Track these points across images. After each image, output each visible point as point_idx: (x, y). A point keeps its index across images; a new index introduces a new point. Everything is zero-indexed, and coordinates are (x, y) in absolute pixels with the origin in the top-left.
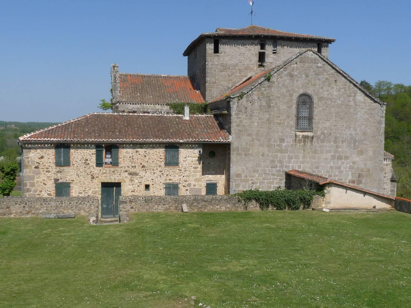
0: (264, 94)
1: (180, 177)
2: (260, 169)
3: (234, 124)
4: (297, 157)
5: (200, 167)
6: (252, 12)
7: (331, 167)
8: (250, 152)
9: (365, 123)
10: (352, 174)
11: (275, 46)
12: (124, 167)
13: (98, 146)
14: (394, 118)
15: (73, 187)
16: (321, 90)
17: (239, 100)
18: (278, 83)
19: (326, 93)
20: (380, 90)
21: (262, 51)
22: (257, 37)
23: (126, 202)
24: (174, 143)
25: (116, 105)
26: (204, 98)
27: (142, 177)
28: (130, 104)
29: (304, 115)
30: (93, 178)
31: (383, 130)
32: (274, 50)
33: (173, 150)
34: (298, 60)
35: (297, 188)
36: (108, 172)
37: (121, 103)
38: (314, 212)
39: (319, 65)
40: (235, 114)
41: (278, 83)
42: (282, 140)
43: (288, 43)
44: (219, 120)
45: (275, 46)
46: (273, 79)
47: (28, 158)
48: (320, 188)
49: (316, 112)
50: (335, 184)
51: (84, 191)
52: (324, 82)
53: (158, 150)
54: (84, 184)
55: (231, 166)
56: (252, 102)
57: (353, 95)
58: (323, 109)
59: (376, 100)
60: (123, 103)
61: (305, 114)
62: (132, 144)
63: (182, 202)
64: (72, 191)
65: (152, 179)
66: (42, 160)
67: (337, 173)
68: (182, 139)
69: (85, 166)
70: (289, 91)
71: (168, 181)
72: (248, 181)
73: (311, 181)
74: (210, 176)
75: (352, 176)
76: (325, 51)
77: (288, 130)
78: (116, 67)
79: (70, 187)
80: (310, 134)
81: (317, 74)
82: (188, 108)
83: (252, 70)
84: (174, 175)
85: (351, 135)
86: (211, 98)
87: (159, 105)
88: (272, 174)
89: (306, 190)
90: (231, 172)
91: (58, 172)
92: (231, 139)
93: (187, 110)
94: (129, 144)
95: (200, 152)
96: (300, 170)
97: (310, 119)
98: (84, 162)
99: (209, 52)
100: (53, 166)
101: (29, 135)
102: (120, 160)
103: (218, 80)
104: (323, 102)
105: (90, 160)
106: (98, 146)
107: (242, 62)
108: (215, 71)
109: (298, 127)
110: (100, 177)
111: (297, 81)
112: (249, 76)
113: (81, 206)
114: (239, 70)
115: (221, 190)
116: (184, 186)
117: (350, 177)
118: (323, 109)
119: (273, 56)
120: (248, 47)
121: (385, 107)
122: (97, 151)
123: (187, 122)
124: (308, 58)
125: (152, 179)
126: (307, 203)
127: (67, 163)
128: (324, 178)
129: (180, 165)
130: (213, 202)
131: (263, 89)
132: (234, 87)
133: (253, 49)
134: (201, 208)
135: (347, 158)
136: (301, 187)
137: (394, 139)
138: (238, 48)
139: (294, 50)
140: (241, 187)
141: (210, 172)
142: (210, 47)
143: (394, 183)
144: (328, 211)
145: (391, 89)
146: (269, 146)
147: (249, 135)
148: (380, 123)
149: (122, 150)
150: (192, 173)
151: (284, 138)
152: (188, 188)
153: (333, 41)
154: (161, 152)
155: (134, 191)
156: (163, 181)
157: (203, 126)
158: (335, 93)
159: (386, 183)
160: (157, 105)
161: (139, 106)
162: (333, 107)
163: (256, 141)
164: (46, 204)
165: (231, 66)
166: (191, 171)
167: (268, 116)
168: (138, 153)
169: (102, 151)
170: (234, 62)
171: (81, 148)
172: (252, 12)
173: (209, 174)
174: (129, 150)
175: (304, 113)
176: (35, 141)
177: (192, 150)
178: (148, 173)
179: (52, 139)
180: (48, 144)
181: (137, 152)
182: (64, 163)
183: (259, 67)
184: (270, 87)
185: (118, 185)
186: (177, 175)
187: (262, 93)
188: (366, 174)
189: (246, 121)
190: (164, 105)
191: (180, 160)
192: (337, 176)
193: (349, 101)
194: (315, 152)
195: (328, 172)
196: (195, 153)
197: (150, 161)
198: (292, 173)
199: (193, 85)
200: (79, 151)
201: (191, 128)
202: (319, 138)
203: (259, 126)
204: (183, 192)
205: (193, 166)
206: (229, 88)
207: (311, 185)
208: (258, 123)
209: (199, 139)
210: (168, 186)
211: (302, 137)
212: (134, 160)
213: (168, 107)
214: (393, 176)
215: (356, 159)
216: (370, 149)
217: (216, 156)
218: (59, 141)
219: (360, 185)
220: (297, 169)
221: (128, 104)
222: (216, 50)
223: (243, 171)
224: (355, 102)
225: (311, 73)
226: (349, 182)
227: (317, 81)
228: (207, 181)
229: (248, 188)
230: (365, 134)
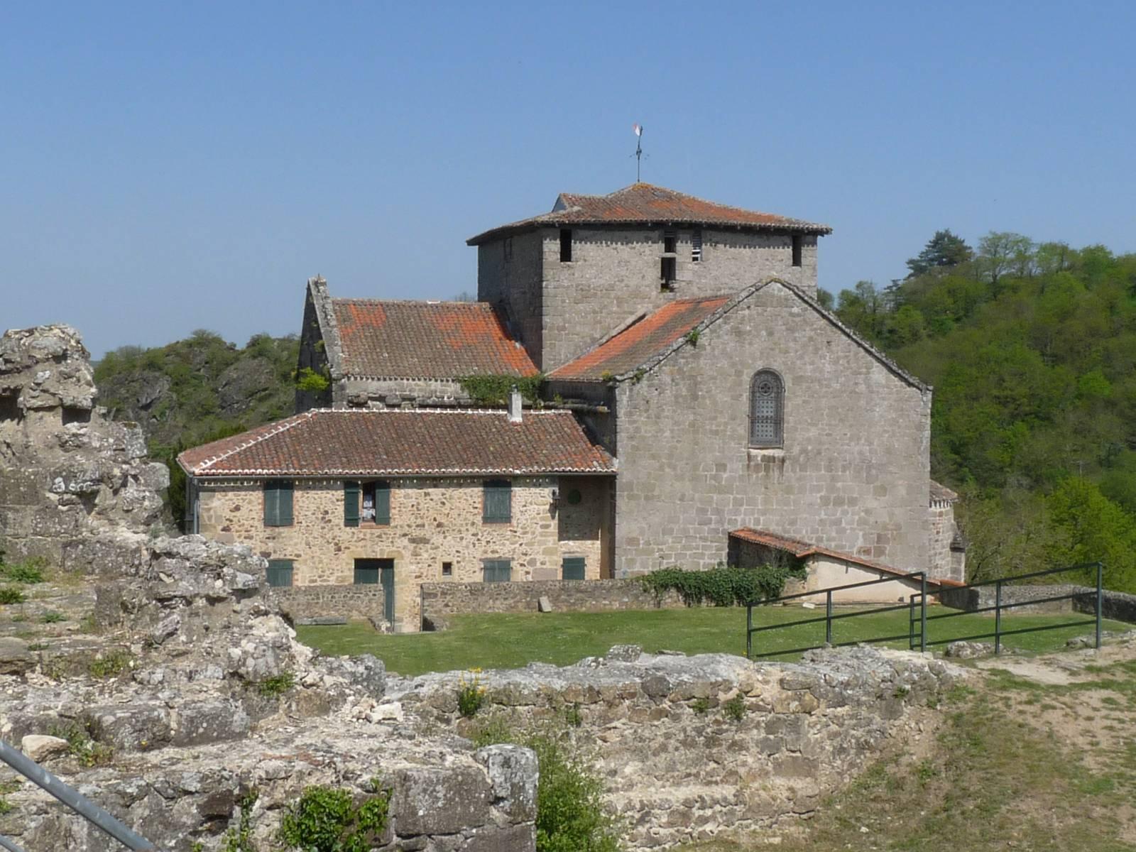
0: (684, 372)
1: (513, 547)
2: (676, 527)
3: (623, 434)
4: (751, 502)
5: (554, 524)
6: (639, 152)
7: (821, 520)
8: (656, 493)
9: (890, 429)
10: (864, 535)
11: (698, 244)
12: (401, 527)
13: (349, 484)
14: (1038, 353)
15: (298, 569)
16: (798, 362)
17: (633, 384)
18: (713, 349)
19: (809, 367)
20: (995, 263)
21: (669, 255)
22: (658, 225)
23: (435, 595)
24: (502, 476)
25: (339, 383)
26: (538, 364)
27: (437, 548)
28: (373, 379)
29: (765, 414)
30: (339, 550)
31: (926, 443)
32: (694, 253)
33: (500, 489)
34: (751, 300)
35: (753, 566)
36: (368, 536)
37: (352, 379)
38: (787, 609)
39: (795, 310)
40: (625, 414)
41: (713, 349)
42: (721, 467)
43: (728, 235)
44: (584, 423)
45: (698, 244)
46: (703, 341)
47: (209, 509)
48: (797, 564)
49: (789, 406)
50: (826, 555)
51: (320, 577)
52: (804, 346)
53: (468, 490)
54: (321, 562)
55: (617, 521)
56: (660, 389)
57: (864, 370)
58: (804, 402)
59: (911, 380)
60: (356, 379)
61: (767, 410)
62: (416, 478)
63: (540, 594)
64: (296, 577)
65: (458, 552)
66: (238, 514)
67: (834, 534)
68: (519, 468)
69: (323, 525)
70: (733, 365)
71: (490, 555)
72: (652, 552)
73: (781, 551)
74: (571, 543)
75: (865, 539)
76: (810, 253)
77: (733, 445)
78: (324, 284)
79: (292, 569)
80: (777, 453)
81: (791, 330)
82: (520, 397)
83: (644, 297)
84: (501, 543)
85: (861, 453)
86: (554, 365)
87: (436, 381)
88: (701, 538)
89: (772, 567)
90: (617, 534)
91: (268, 538)
92: (616, 465)
93: (517, 400)
94: (411, 479)
95: (554, 493)
96: (759, 528)
97: (778, 421)
98: (320, 516)
99: (550, 259)
100: (260, 525)
101: (209, 463)
102: (393, 511)
103: (569, 322)
104: (804, 385)
105: (333, 513)
106: (349, 484)
107: (623, 280)
108: (563, 301)
109: (755, 439)
110: (353, 548)
111: (750, 344)
112: (640, 314)
113: (352, 602)
114: (617, 298)
115: (593, 570)
116: (522, 565)
117: (860, 543)
118: (804, 402)
119: (692, 266)
120: (638, 246)
121: (930, 395)
122: (346, 493)
123: (518, 428)
124: (773, 296)
125: (458, 552)
126: (773, 593)
127: (287, 520)
128: (805, 545)
129: (514, 522)
130: (597, 593)
131: (682, 361)
132: (606, 338)
133: (647, 252)
134: (574, 604)
135: (853, 502)
136: (761, 562)
137: (1037, 422)
138: (616, 249)
139: (739, 253)
140: (638, 564)
141: (570, 535)
142: (552, 248)
143: (957, 554)
144: (812, 606)
145: (1030, 258)
146: (695, 479)
147: (653, 457)
148: (920, 427)
149: (397, 491)
150: (539, 538)
151: (724, 461)
152: (530, 569)
153: (827, 232)
154: (475, 495)
155: (420, 577)
156: (479, 556)
157: (554, 436)
158: (828, 368)
159: (940, 553)
160: (433, 382)
161: (392, 384)
162: (824, 397)
163: (667, 470)
164: (288, 599)
165: (598, 293)
166: (537, 533)
167: (692, 417)
168: (428, 498)
169: (357, 493)
170: (605, 280)
171: (314, 489)
172: (639, 152)
173: (569, 539)
174: (410, 491)
175: (765, 410)
176: (226, 474)
177: (538, 490)
178: (449, 538)
179: (259, 471)
180: (249, 480)
181: (427, 494)
182: (281, 520)
183: (662, 291)
184: (696, 357)
185: (388, 564)
186: (507, 542)
187: (680, 371)
188: (892, 534)
189: (648, 428)
190: (448, 381)
191: (513, 510)
192: (834, 539)
193: (856, 384)
194: (789, 490)
195: (814, 531)
196: (545, 495)
197: (454, 513)
198: (742, 535)
199: (503, 327)
200: (312, 493)
201: (531, 442)
202: (795, 460)
203: (673, 437)
204: (519, 575)
205: (541, 523)
206: (594, 340)
207: (781, 559)
208: (672, 431)
209: (553, 467)
210: (488, 565)
211: (762, 460)
212: (422, 512)
213: (458, 385)
214: (955, 539)
215: (872, 503)
216: (900, 482)
217: (586, 502)
218: (272, 474)
219: (882, 558)
220: (752, 527)
221: (367, 379)
222: (566, 255)
223: (642, 532)
224: (869, 386)
225: (780, 327)
226: (859, 552)
227: (791, 344)
228: (565, 553)
229: (653, 566)
230: (889, 451)
